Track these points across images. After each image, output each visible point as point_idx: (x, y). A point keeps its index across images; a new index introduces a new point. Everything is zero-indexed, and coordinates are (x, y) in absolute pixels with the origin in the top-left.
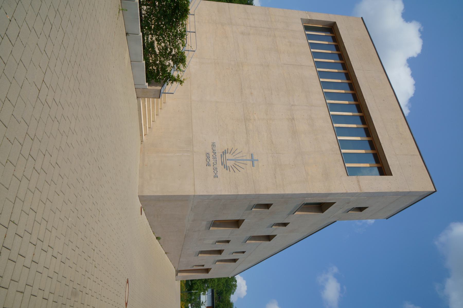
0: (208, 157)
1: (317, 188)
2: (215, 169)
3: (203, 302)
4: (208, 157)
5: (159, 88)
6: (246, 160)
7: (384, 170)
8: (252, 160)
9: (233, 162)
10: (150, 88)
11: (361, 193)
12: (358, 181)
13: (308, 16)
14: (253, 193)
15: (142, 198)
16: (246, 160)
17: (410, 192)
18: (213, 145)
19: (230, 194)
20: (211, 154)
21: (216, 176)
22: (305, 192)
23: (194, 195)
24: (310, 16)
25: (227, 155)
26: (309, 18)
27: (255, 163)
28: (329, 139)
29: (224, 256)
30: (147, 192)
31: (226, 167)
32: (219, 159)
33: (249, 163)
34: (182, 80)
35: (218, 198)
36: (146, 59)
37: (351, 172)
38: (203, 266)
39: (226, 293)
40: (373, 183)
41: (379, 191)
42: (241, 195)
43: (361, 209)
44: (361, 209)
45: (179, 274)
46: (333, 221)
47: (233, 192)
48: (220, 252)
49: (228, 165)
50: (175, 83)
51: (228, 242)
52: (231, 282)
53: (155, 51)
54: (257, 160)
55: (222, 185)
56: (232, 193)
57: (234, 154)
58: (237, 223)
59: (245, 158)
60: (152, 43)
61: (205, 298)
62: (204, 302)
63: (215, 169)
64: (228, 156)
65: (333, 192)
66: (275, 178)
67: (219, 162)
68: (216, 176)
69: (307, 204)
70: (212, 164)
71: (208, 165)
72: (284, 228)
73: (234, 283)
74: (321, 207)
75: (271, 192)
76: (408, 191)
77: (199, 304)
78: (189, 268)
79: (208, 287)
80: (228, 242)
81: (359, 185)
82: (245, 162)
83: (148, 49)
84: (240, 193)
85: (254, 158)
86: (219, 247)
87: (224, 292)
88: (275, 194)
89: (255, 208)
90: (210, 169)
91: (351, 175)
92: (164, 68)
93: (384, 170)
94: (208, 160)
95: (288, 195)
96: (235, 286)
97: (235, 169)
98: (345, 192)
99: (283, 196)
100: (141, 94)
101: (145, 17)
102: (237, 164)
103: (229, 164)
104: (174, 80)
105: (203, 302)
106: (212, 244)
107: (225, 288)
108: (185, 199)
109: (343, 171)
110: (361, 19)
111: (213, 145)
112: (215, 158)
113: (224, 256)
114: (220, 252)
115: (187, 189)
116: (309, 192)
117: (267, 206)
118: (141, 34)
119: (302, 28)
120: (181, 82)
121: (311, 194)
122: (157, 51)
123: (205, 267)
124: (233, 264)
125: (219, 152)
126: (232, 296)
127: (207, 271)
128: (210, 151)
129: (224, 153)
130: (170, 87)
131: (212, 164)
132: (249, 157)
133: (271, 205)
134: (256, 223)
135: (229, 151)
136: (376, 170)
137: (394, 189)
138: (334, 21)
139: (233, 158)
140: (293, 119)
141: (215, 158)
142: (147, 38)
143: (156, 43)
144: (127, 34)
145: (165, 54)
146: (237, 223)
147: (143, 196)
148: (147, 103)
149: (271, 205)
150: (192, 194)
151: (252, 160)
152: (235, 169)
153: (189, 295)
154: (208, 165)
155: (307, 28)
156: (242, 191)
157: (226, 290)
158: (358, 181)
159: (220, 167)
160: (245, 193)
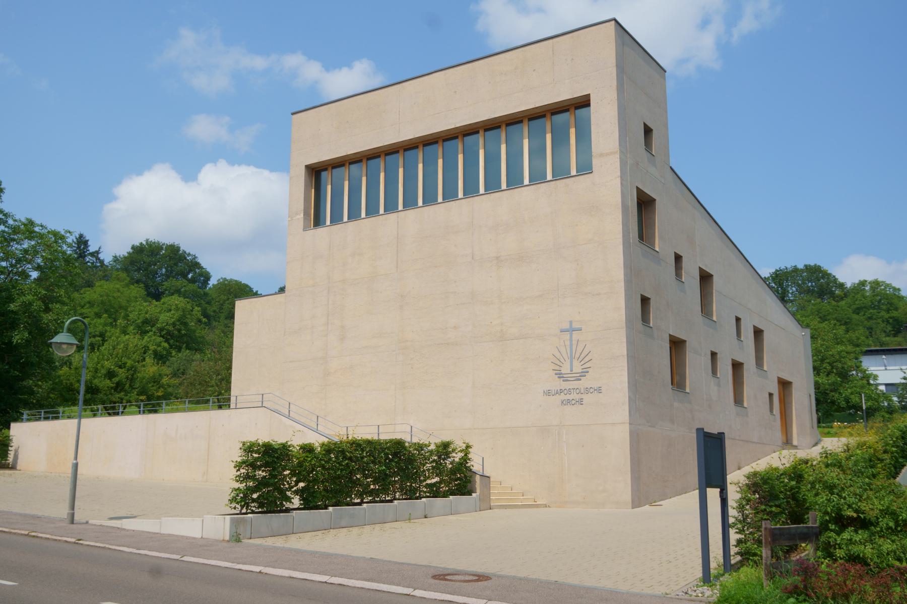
1: (612, 223)
2: (587, 391)
3: (905, 378)
5: (478, 478)
6: (571, 340)
7: (583, 103)
8: (571, 330)
9: (575, 363)
10: (478, 491)
11: (621, 152)
12: (601, 155)
13: (298, 217)
16: (571, 340)
18: (548, 393)
19: (626, 368)
20: (563, 397)
21: (599, 390)
23: (630, 424)
24: (297, 214)
26: (302, 215)
27: (575, 325)
29: (748, 357)
30: (627, 496)
31: (584, 373)
32: (571, 384)
33: (576, 335)
34: (465, 445)
35: (634, 385)
37: (585, 168)
38: (771, 395)
40: (604, 121)
41: (617, 122)
43: (648, 131)
45: (795, 443)
48: (737, 367)
49: (580, 371)
51: (714, 355)
54: (571, 322)
55: (613, 379)
57: (562, 360)
58: (677, 345)
59: (568, 343)
60: (428, 486)
61: (887, 372)
62: (903, 375)
63: (587, 391)
64: (565, 369)
66: (599, 294)
68: (599, 390)
69: (641, 237)
71: (581, 401)
73: (867, 288)
74: (645, 204)
75: (622, 303)
76: (615, 69)
77: (906, 387)
79: (858, 368)
80: (714, 355)
82: (574, 343)
83: (435, 492)
85: (568, 327)
86: (725, 369)
87: (895, 314)
88: (626, 295)
89: (651, 245)
90: (587, 398)
92: (453, 471)
93: (583, 103)
94: (573, 402)
95: (625, 275)
96: (876, 284)
97: (587, 359)
98: (618, 180)
99: (628, 282)
100: (486, 505)
101: (405, 494)
102: (577, 356)
103: (577, 368)
106: (719, 385)
107: (883, 313)
109: (585, 180)
110: (295, 116)
111: (548, 393)
112: (569, 391)
113: (748, 357)
114: (737, 367)
115: (621, 435)
116: (621, 240)
117: (645, 301)
118: (424, 500)
119: (320, 231)
120: (468, 447)
121: (624, 236)
122: (437, 479)
123: (775, 389)
124: (766, 336)
127: (785, 385)
129: (560, 375)
130: (475, 465)
131: (580, 396)
132: (567, 336)
133: (645, 125)
135: (557, 368)
136: (581, 112)
137: (612, 94)
138: (304, 168)
140: (497, 258)
142: (425, 492)
143: (429, 482)
144: (426, 517)
145: (438, 469)
146: (677, 345)
147: (633, 502)
149: (645, 125)
150: (627, 427)
151: (571, 330)
152: (587, 359)
153: (877, 414)
154: (581, 401)
155: (318, 221)
156: (620, 348)
157: (888, 311)
158: (601, 155)
159: (584, 383)
160: (625, 344)
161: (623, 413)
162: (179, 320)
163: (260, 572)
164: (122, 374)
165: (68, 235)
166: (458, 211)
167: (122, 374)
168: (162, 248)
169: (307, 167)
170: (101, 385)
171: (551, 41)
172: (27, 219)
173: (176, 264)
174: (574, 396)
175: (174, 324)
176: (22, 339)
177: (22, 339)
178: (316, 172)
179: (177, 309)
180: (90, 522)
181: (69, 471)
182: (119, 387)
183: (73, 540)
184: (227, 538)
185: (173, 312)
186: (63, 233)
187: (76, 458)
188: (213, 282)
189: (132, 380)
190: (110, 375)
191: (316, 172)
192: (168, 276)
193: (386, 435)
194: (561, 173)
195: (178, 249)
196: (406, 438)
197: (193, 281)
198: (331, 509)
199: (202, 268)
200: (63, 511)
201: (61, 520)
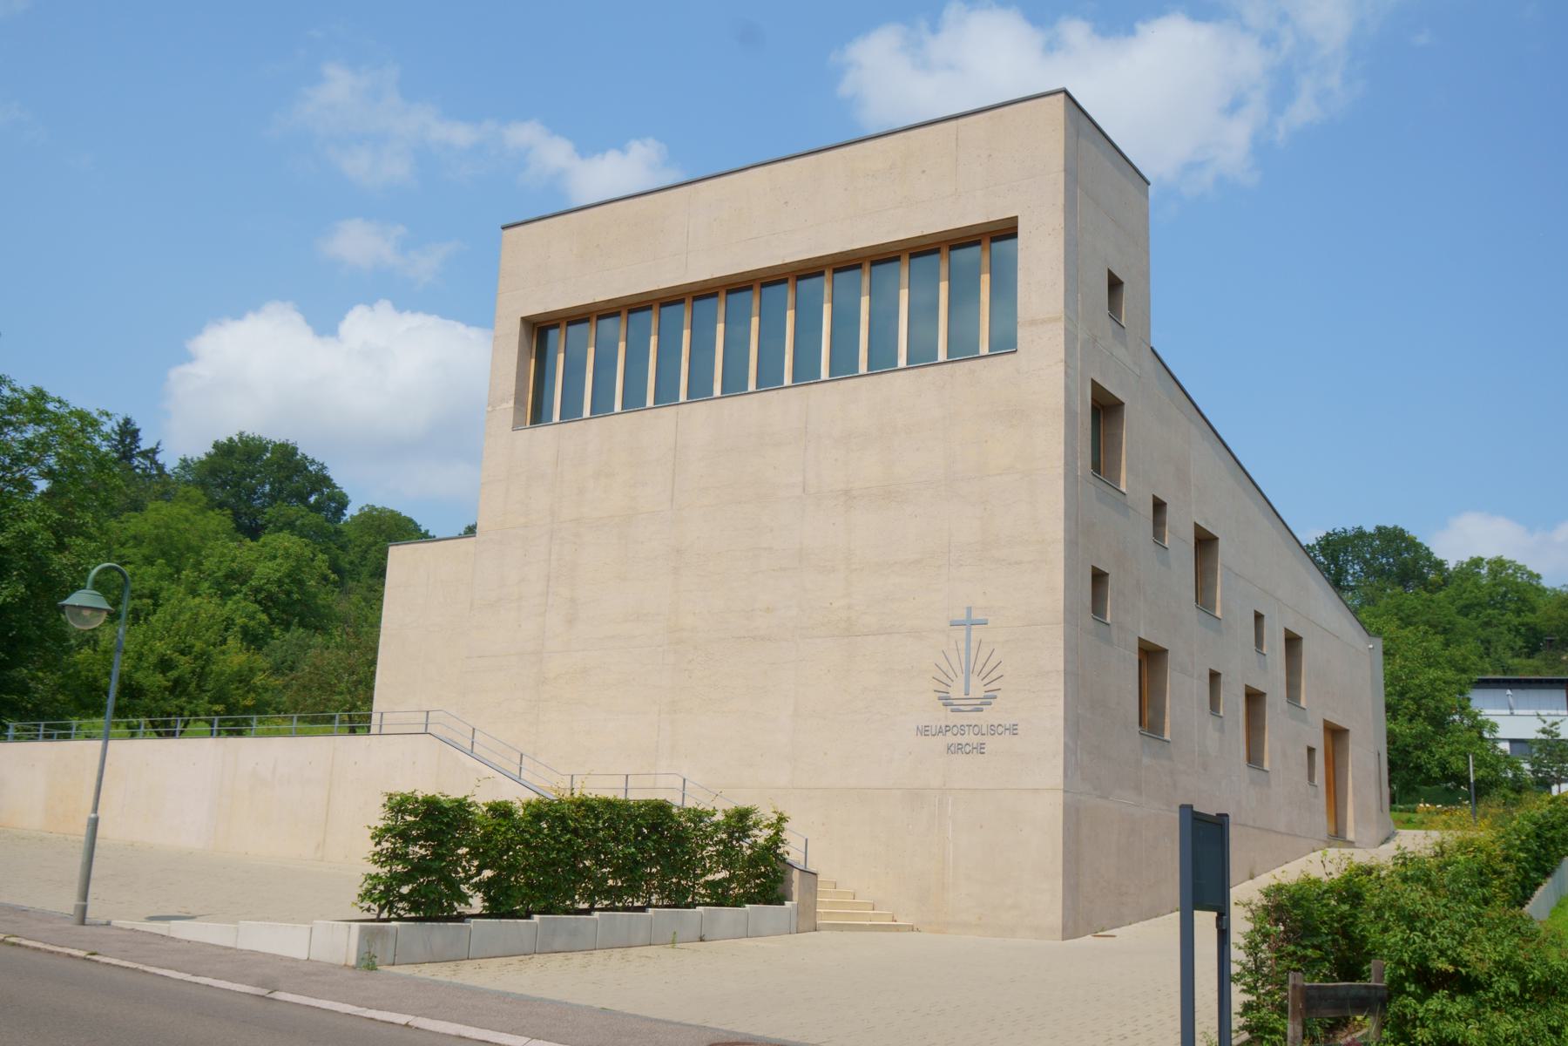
0: (959, 748)
1: (1046, 440)
2: (993, 730)
3: (1544, 731)
4: (959, 748)
5: (796, 875)
7: (1006, 231)
8: (969, 623)
10: (795, 897)
11: (1068, 318)
12: (1033, 323)
13: (505, 405)
14: (1059, 631)
15: (1071, 930)
17: (1065, 170)
18: (924, 731)
20: (950, 738)
21: (1013, 730)
22: (1061, 482)
25: (952, 695)
27: (977, 616)
28: (902, 390)
29: (1273, 683)
31: (988, 699)
32: (965, 714)
33: (976, 632)
35: (1074, 726)
36: (737, 903)
37: (1005, 344)
38: (1311, 751)
39: (1533, 610)
40: (1040, 262)
41: (1062, 267)
42: (1066, 662)
43: (1115, 284)
44: (1115, 284)
45: (1350, 836)
46: (1149, 363)
47: (1057, 686)
48: (1254, 699)
50: (784, 836)
51: (1214, 676)
52: (1479, 587)
53: (724, 879)
54: (969, 609)
55: (1038, 710)
56: (1061, 687)
57: (951, 675)
58: (1151, 657)
59: (962, 645)
60: (708, 884)
61: (1513, 720)
62: (1541, 725)
63: (993, 730)
64: (956, 691)
65: (1062, 401)
67: (973, 718)
68: (1013, 730)
69: (1096, 467)
70: (979, 739)
71: (980, 749)
72: (1170, 509)
73: (1484, 572)
74: (1105, 409)
77: (1557, 755)
78: (1322, 800)
80: (1214, 676)
81: (1043, 322)
82: (974, 645)
83: (720, 897)
84: (1061, 666)
85: (964, 617)
87: (1529, 618)
90: (992, 743)
91: (1015, 345)
93: (1006, 231)
94: (968, 749)
96: (1499, 565)
97: (994, 675)
98: (1061, 367)
99: (1071, 544)
100: (808, 922)
102: (978, 667)
103: (978, 690)
104: (776, 841)
105: (1544, 731)
106: (1221, 730)
107: (1509, 616)
108: (1073, 817)
109: (1004, 363)
111: (924, 731)
112: (962, 730)
113: (1273, 683)
114: (1254, 699)
115: (1048, 809)
116: (1061, 471)
117: (1099, 578)
119: (542, 432)
120: (781, 819)
121: (1066, 464)
122: (724, 874)
123: (1319, 742)
124: (1307, 647)
125: (946, 717)
126: (1546, 583)
128: (942, 741)
129: (947, 701)
130: (793, 851)
131: (979, 739)
132: (961, 633)
134: (1155, 598)
135: (942, 688)
137: (1056, 219)
138: (518, 322)
139: (962, 677)
140: (847, 492)
141: (962, 730)
143: (710, 877)
145: (727, 856)
146: (1151, 657)
147: (1064, 928)
148: (826, 903)
151: (969, 623)
152: (994, 675)
154: (980, 749)
156: (1055, 659)
157: (1518, 612)
158: (1033, 323)
159: (987, 717)
160: (1061, 652)
161: (1051, 772)
162: (289, 576)
163: (406, 1025)
164: (185, 664)
165: (104, 419)
166: (784, 407)
167: (185, 664)
168: (266, 449)
169: (523, 319)
170: (146, 683)
171: (953, 123)
172: (35, 389)
173: (289, 478)
174: (970, 738)
175: (280, 582)
176: (14, 596)
177: (14, 596)
178: (539, 330)
179: (287, 556)
180: (115, 922)
181: (82, 830)
182: (178, 687)
183: (82, 954)
184: (353, 961)
185: (279, 561)
186: (95, 415)
187: (95, 810)
188: (352, 511)
189: (202, 675)
190: (165, 665)
191: (539, 330)
192: (273, 498)
193: (640, 792)
194: (962, 349)
195: (294, 451)
196: (675, 799)
197: (317, 508)
198: (536, 918)
199: (334, 486)
200: (67, 902)
201: (64, 918)
